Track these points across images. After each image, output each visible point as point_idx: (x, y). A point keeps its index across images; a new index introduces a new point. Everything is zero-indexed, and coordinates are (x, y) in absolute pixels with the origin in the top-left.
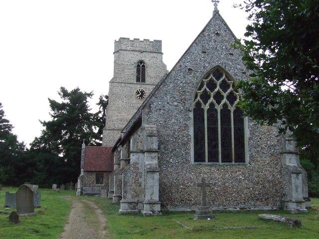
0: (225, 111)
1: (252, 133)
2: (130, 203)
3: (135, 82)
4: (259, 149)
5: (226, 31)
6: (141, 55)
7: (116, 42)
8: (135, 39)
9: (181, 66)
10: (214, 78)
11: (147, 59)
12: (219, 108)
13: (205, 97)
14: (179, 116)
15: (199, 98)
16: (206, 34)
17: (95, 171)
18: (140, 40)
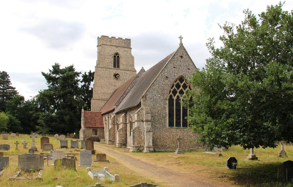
2: (136, 147)
3: (113, 68)
5: (186, 56)
8: (112, 37)
10: (179, 82)
11: (122, 52)
13: (175, 92)
14: (161, 103)
15: (171, 93)
16: (176, 57)
17: (92, 127)
18: (116, 38)
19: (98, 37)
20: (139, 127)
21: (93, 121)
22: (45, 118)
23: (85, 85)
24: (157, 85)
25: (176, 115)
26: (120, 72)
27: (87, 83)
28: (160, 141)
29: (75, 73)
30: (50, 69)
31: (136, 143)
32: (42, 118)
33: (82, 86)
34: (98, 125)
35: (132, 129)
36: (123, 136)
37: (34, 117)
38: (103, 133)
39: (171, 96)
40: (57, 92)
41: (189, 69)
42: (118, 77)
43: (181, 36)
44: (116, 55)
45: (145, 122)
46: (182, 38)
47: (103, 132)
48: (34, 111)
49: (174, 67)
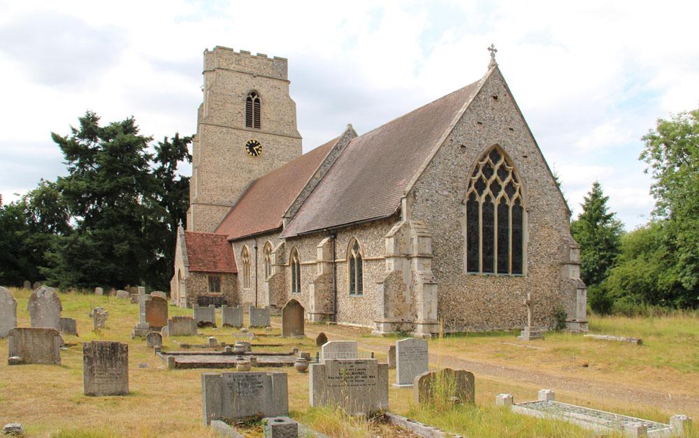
0: (503, 207)
1: (531, 238)
3: (244, 127)
4: (538, 258)
6: (254, 81)
7: (207, 52)
8: (242, 52)
9: (452, 140)
11: (266, 91)
12: (496, 202)
13: (480, 186)
14: (451, 211)
17: (207, 273)
19: (207, 50)
20: (400, 272)
21: (210, 257)
22: (66, 247)
23: (162, 170)
24: (441, 167)
25: (483, 242)
26: (262, 139)
27: (169, 164)
28: (447, 307)
29: (139, 137)
30: (74, 127)
31: (391, 314)
32: (60, 246)
33: (157, 172)
34: (221, 268)
35: (270, 274)
36: (326, 294)
37: (27, 245)
38: (234, 286)
39: (472, 196)
40: (96, 183)
41: (511, 129)
42: (257, 150)
43: (492, 46)
44: (251, 96)
45: (415, 261)
46: (496, 51)
47: (236, 284)
48: (28, 231)
49: (479, 123)
